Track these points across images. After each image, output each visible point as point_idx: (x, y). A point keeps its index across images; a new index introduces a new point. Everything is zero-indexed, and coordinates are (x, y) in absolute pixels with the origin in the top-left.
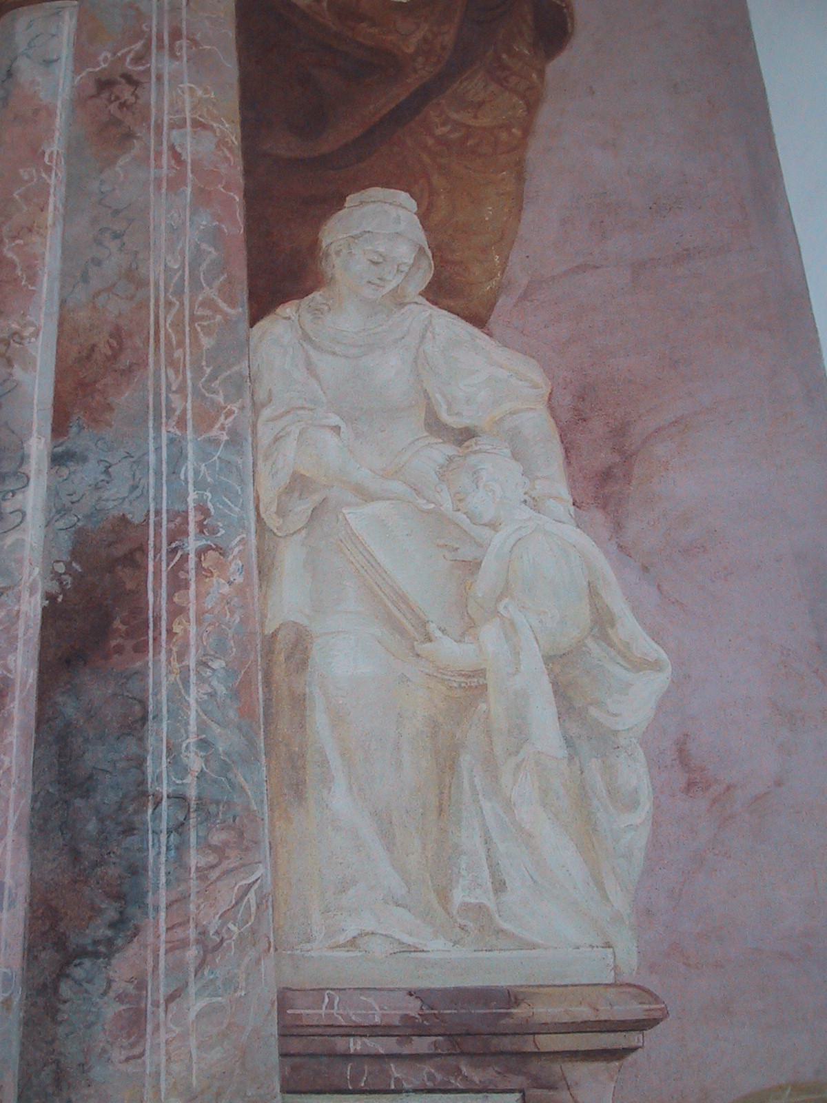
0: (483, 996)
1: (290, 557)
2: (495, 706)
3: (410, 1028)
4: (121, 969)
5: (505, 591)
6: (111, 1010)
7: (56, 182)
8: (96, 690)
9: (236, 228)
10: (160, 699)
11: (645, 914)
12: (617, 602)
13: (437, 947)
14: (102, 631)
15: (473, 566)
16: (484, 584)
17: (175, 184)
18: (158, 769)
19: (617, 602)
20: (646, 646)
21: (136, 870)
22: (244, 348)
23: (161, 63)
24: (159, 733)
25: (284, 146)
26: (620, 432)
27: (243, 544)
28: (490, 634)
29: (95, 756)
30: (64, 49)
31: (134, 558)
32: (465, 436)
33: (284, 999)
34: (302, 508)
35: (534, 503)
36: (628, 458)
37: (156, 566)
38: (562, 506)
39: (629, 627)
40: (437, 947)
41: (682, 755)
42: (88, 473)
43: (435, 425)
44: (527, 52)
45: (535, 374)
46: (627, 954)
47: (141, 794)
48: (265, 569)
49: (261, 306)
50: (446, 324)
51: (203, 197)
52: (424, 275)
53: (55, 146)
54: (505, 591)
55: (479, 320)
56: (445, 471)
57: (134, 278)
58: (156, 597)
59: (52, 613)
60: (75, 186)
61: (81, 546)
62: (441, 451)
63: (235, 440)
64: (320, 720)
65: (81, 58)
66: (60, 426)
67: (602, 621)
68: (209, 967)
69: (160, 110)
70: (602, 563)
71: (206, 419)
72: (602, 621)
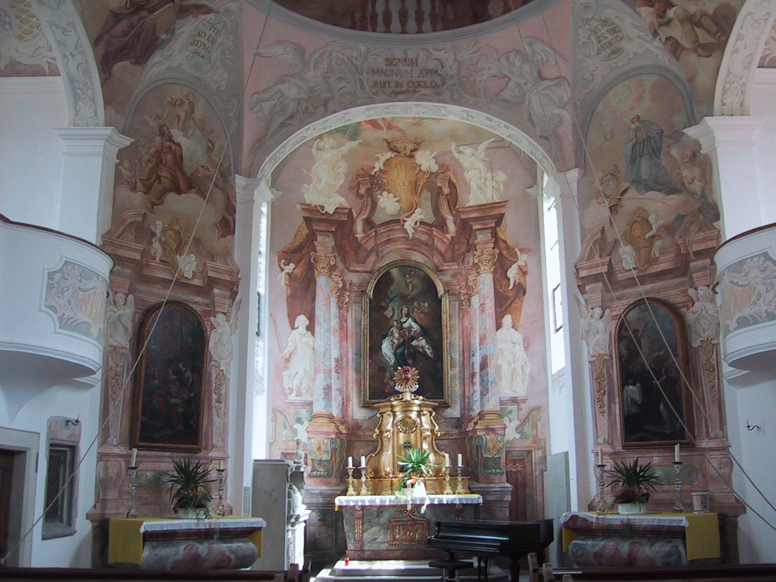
0: (515, 397)
1: (500, 357)
2: (516, 371)
3: (509, 400)
4: (487, 396)
5: (518, 360)
6: (487, 400)
7: (478, 318)
8: (484, 372)
9: (494, 321)
10: (489, 372)
11: (527, 390)
12: (527, 360)
13: (512, 394)
14: (484, 366)
15: (515, 357)
16: (516, 359)
17: (489, 316)
18: (490, 380)
19: (527, 360)
20: (529, 365)
21: (488, 388)
22: (495, 335)
23: (487, 301)
24: (489, 375)
25: (499, 310)
26: (528, 342)
27: (496, 356)
28: (516, 364)
29: (485, 378)
30: (477, 300)
31: (487, 359)
32: (515, 343)
33: (500, 398)
34: (501, 352)
35: (521, 350)
36: (529, 345)
37: (489, 359)
38: (523, 351)
39: (528, 363)
40: (512, 394)
41: (531, 376)
42: (482, 350)
43: (513, 343)
44: (662, 406)
45: (520, 335)
46: (526, 394)
47: (488, 381)
48: (498, 358)
49: (497, 329)
50: (513, 330)
51: (491, 318)
52: (511, 325)
53: (477, 314)
54: (518, 360)
55: (516, 330)
56: (513, 347)
57: (486, 328)
58: (489, 362)
59: (480, 365)
60: (479, 318)
61: (482, 357)
62: (513, 345)
63: (495, 345)
64: (502, 373)
65: (479, 302)
66: (480, 346)
67: (525, 363)
68: (498, 551)
69: (471, 521)
70: (526, 356)
71: (493, 343)
72: (525, 363)
